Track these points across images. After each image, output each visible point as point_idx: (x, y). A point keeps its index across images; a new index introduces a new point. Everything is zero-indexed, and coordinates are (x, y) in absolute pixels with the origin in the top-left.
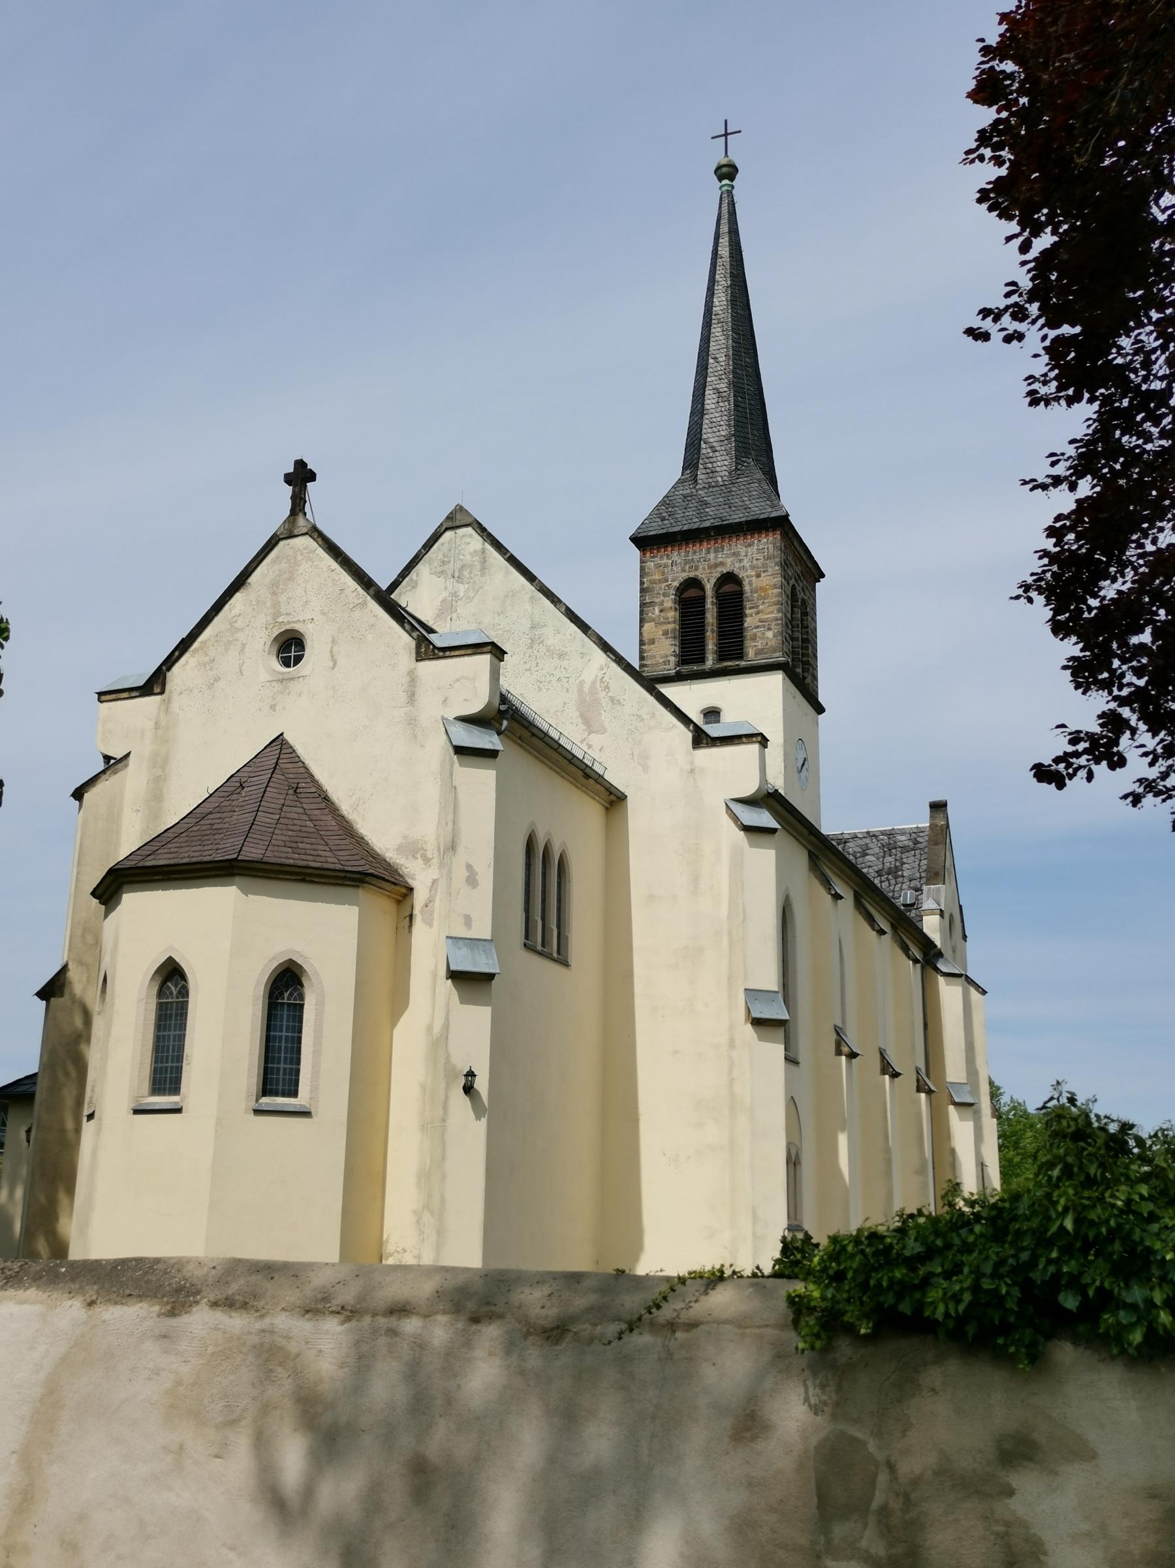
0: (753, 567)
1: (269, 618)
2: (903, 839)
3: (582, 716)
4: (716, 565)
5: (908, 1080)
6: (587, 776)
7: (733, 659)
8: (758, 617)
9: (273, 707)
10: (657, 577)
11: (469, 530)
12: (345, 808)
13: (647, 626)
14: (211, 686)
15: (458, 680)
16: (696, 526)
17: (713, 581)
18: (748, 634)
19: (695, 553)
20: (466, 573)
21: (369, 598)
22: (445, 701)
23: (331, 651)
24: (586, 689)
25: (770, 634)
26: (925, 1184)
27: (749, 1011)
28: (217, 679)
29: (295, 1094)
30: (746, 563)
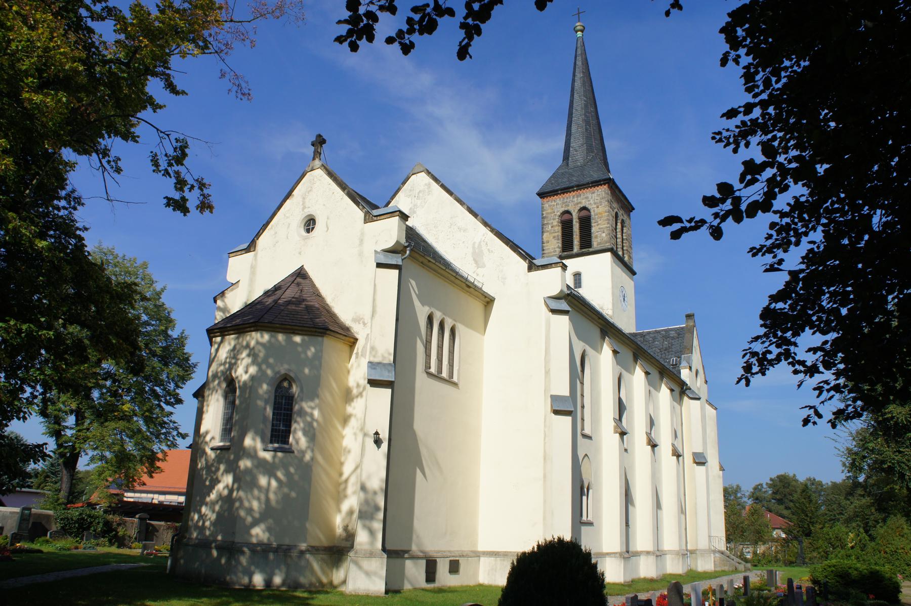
2: (673, 334)
6: (469, 287)
7: (587, 247)
9: (300, 253)
13: (545, 235)
18: (593, 235)
24: (476, 246)
25: (604, 235)
30: (592, 202)
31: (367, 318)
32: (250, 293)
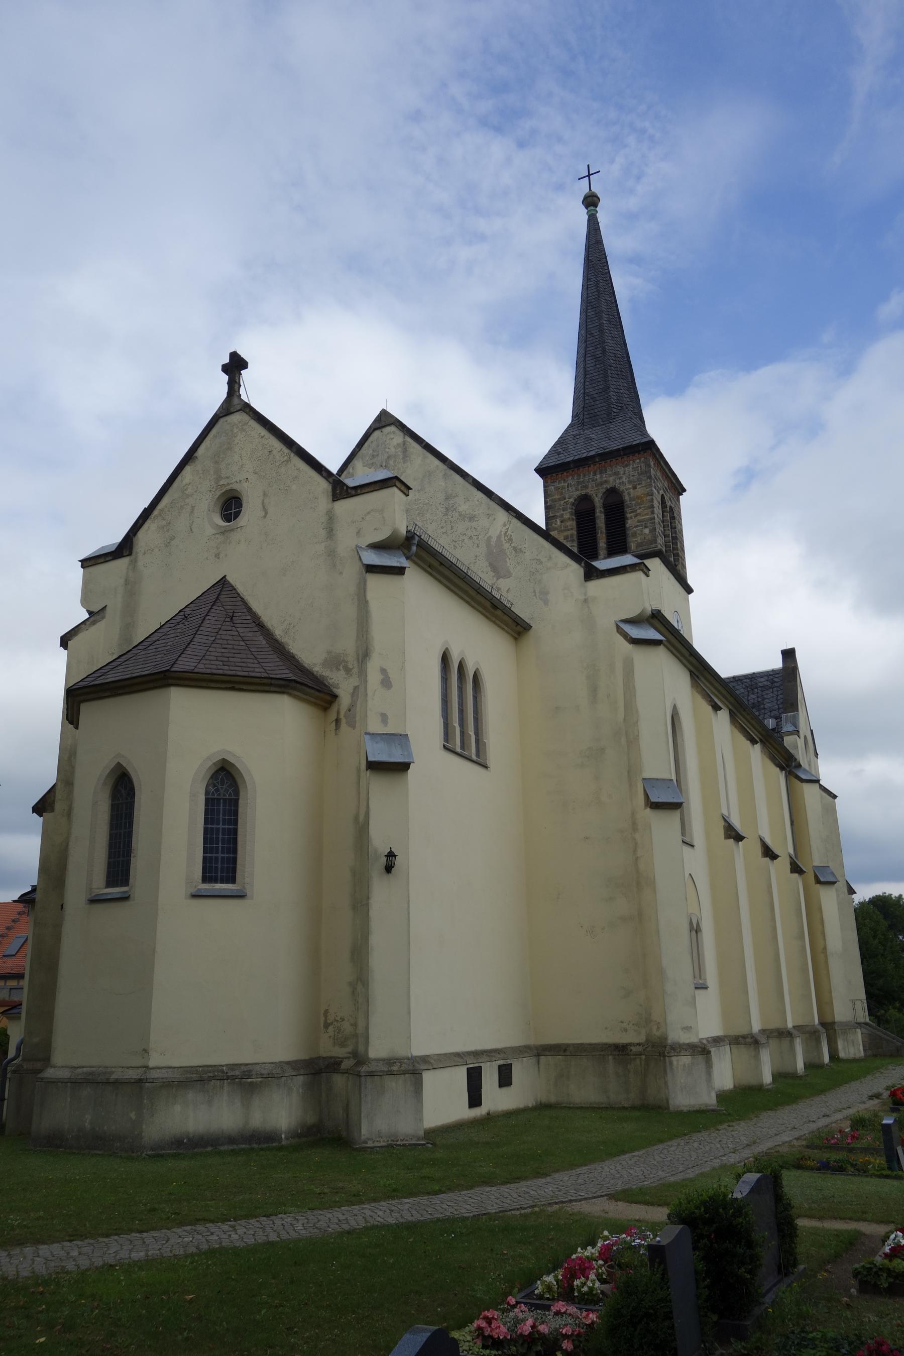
0: (630, 482)
1: (213, 483)
3: (491, 565)
4: (602, 484)
5: (783, 863)
6: (495, 607)
8: (636, 519)
9: (217, 556)
10: (557, 497)
11: (392, 428)
12: (278, 633)
14: (168, 545)
15: (368, 513)
16: (584, 455)
17: (600, 495)
18: (629, 532)
19: (584, 476)
20: (391, 462)
21: (292, 455)
22: (358, 533)
23: (263, 503)
26: (804, 947)
27: (647, 796)
28: (173, 538)
29: (233, 881)
30: (624, 479)
31: (352, 662)
32: (128, 627)
